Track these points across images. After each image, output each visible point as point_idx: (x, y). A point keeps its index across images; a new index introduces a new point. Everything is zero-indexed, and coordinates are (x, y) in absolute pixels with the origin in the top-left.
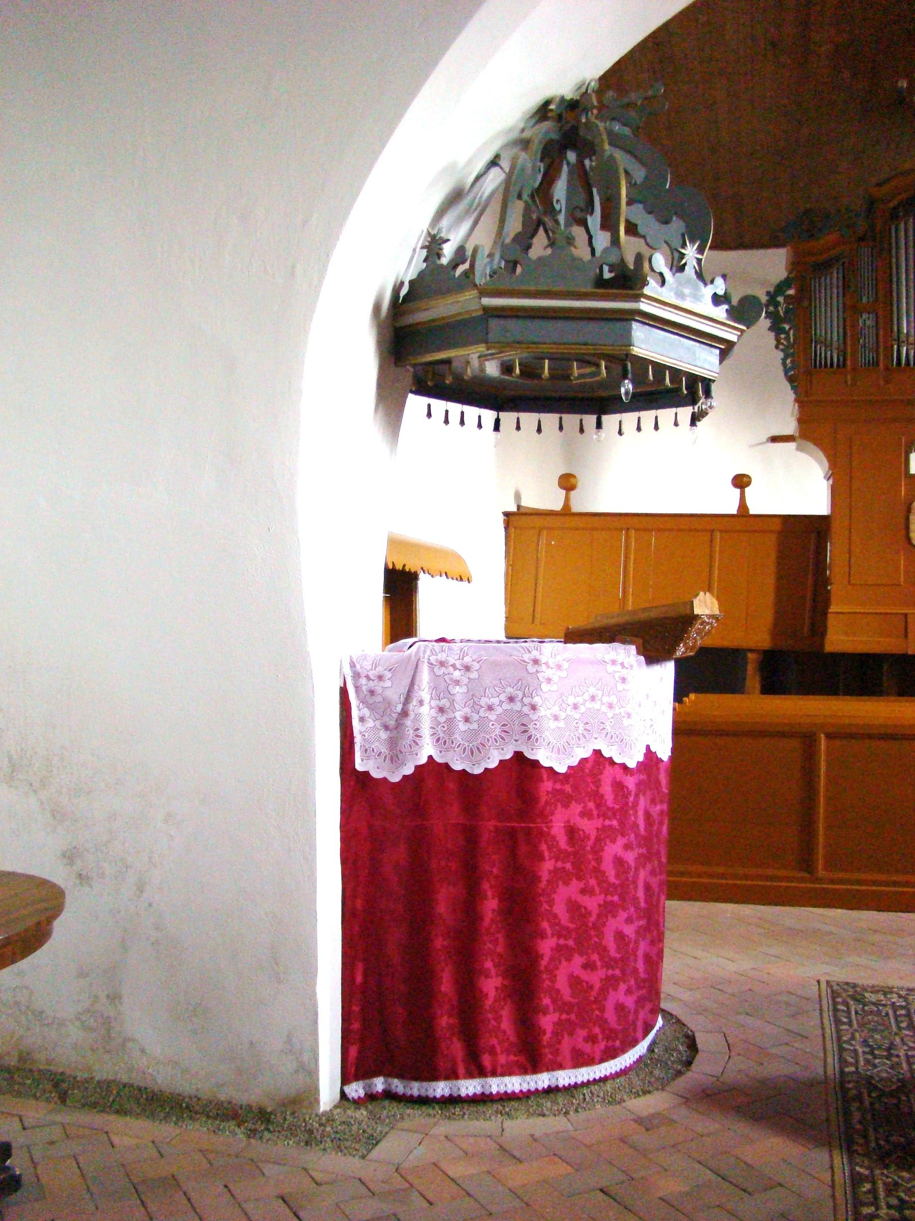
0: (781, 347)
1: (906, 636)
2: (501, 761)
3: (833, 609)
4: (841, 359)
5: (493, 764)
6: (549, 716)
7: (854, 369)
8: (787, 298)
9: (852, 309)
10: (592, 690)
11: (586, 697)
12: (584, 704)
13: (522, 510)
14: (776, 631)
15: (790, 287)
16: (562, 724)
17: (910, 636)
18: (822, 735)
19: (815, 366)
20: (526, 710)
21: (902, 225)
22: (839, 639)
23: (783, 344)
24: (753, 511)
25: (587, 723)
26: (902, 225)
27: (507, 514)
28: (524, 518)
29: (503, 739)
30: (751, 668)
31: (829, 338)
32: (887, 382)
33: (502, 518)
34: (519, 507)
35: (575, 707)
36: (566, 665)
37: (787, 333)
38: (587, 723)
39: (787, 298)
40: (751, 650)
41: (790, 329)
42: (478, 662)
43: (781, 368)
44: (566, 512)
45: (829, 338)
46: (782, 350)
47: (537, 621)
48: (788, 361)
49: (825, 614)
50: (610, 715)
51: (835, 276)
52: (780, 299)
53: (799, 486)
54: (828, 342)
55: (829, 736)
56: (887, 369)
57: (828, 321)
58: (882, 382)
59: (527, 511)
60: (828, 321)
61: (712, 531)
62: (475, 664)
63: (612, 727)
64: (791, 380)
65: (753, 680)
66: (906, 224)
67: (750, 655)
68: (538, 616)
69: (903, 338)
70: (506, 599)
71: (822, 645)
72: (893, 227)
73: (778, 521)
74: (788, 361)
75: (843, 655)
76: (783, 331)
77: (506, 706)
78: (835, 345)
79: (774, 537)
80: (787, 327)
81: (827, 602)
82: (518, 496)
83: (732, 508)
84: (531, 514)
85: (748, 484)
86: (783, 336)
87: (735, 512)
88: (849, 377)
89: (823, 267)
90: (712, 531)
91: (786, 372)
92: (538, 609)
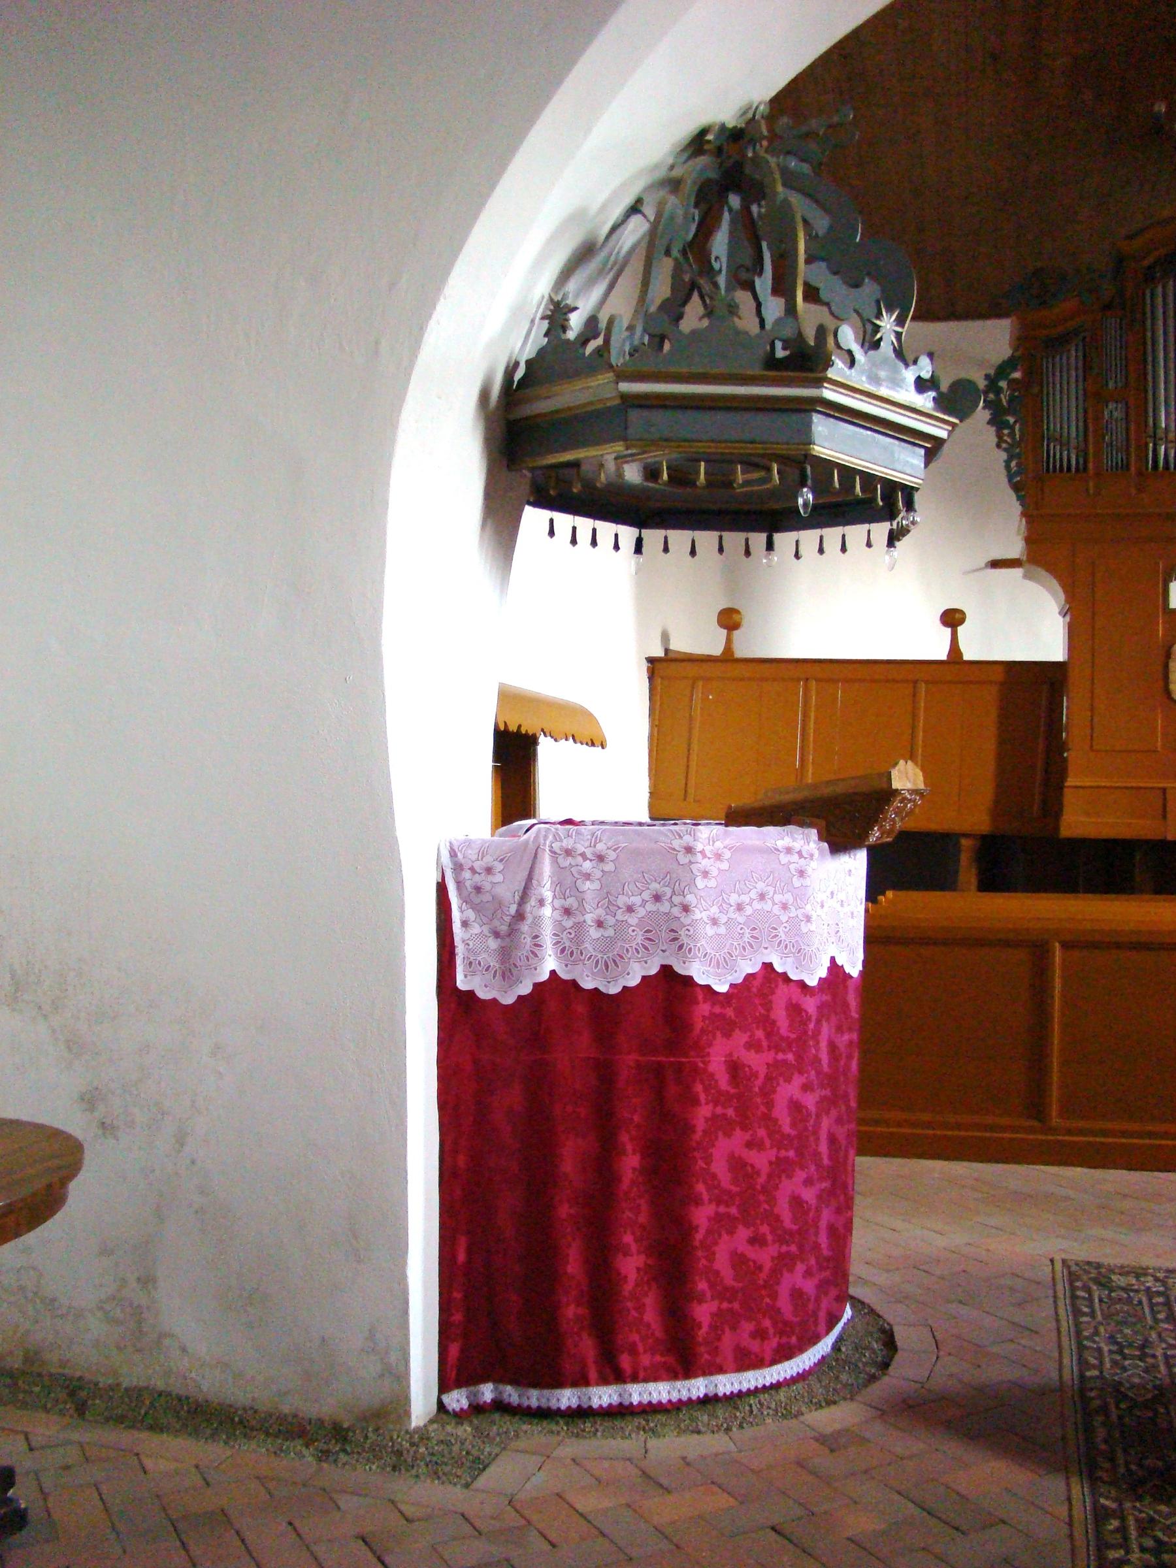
0: (1004, 445)
1: (1164, 816)
2: (644, 978)
3: (1070, 781)
4: (1081, 461)
5: (633, 981)
6: (705, 919)
7: (1098, 474)
8: (1012, 382)
9: (1095, 397)
10: (761, 886)
11: (753, 894)
12: (750, 904)
13: (671, 655)
14: (998, 810)
15: (1015, 369)
16: (722, 930)
17: (1170, 816)
18: (1057, 944)
19: (1048, 470)
20: (676, 911)
21: (1159, 290)
22: (1078, 820)
23: (1006, 442)
24: (968, 656)
25: (754, 929)
26: (1159, 290)
27: (651, 661)
28: (673, 666)
29: (647, 949)
30: (965, 858)
31: (1065, 434)
32: (1140, 490)
33: (645, 665)
34: (667, 651)
35: (740, 908)
36: (727, 854)
37: (1012, 428)
38: (754, 929)
39: (1012, 382)
40: (965, 835)
41: (1015, 422)
42: (615, 850)
43: (1004, 472)
44: (728, 657)
45: (1065, 434)
46: (1005, 450)
47: (691, 798)
48: (1013, 464)
49: (1060, 788)
50: (784, 918)
51: (1074, 354)
52: (1003, 384)
53: (1029, 626)
54: (1065, 439)
55: (1065, 946)
56: (1140, 474)
57: (1065, 412)
58: (1133, 491)
59: (679, 657)
60: (1065, 412)
61: (915, 682)
62: (611, 852)
63: (786, 933)
64: (1016, 488)
65: (968, 873)
66: (1164, 287)
67: (964, 841)
68: (691, 791)
69: (1160, 434)
70: (650, 769)
71: (1057, 828)
72: (1148, 292)
73: (1000, 668)
74: (1013, 464)
75: (1083, 841)
76: (1006, 425)
77: (650, 907)
78: (1073, 442)
79: (994, 690)
80: (1011, 420)
81: (1063, 774)
82: (665, 637)
83: (941, 653)
84: (683, 661)
85: (962, 621)
86: (1006, 432)
87: (944, 657)
88: (1091, 484)
89: (1056, 344)
90: (915, 682)
91: (1010, 477)
92: (692, 782)
